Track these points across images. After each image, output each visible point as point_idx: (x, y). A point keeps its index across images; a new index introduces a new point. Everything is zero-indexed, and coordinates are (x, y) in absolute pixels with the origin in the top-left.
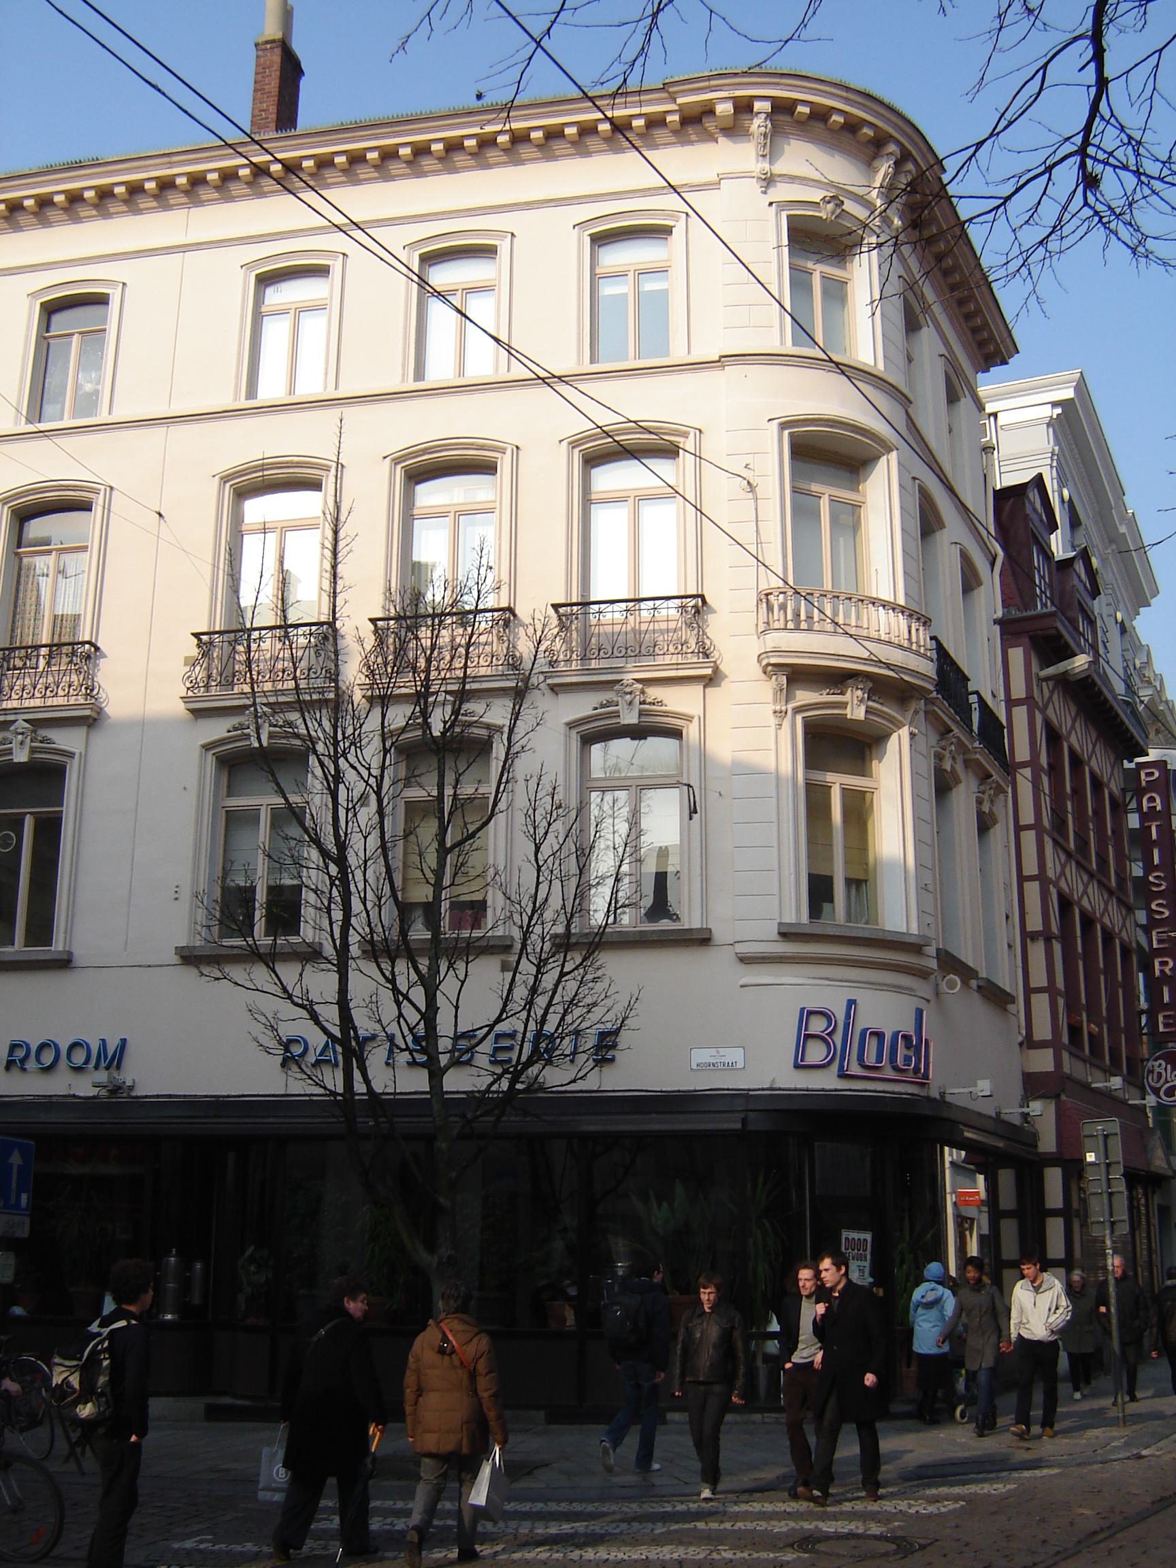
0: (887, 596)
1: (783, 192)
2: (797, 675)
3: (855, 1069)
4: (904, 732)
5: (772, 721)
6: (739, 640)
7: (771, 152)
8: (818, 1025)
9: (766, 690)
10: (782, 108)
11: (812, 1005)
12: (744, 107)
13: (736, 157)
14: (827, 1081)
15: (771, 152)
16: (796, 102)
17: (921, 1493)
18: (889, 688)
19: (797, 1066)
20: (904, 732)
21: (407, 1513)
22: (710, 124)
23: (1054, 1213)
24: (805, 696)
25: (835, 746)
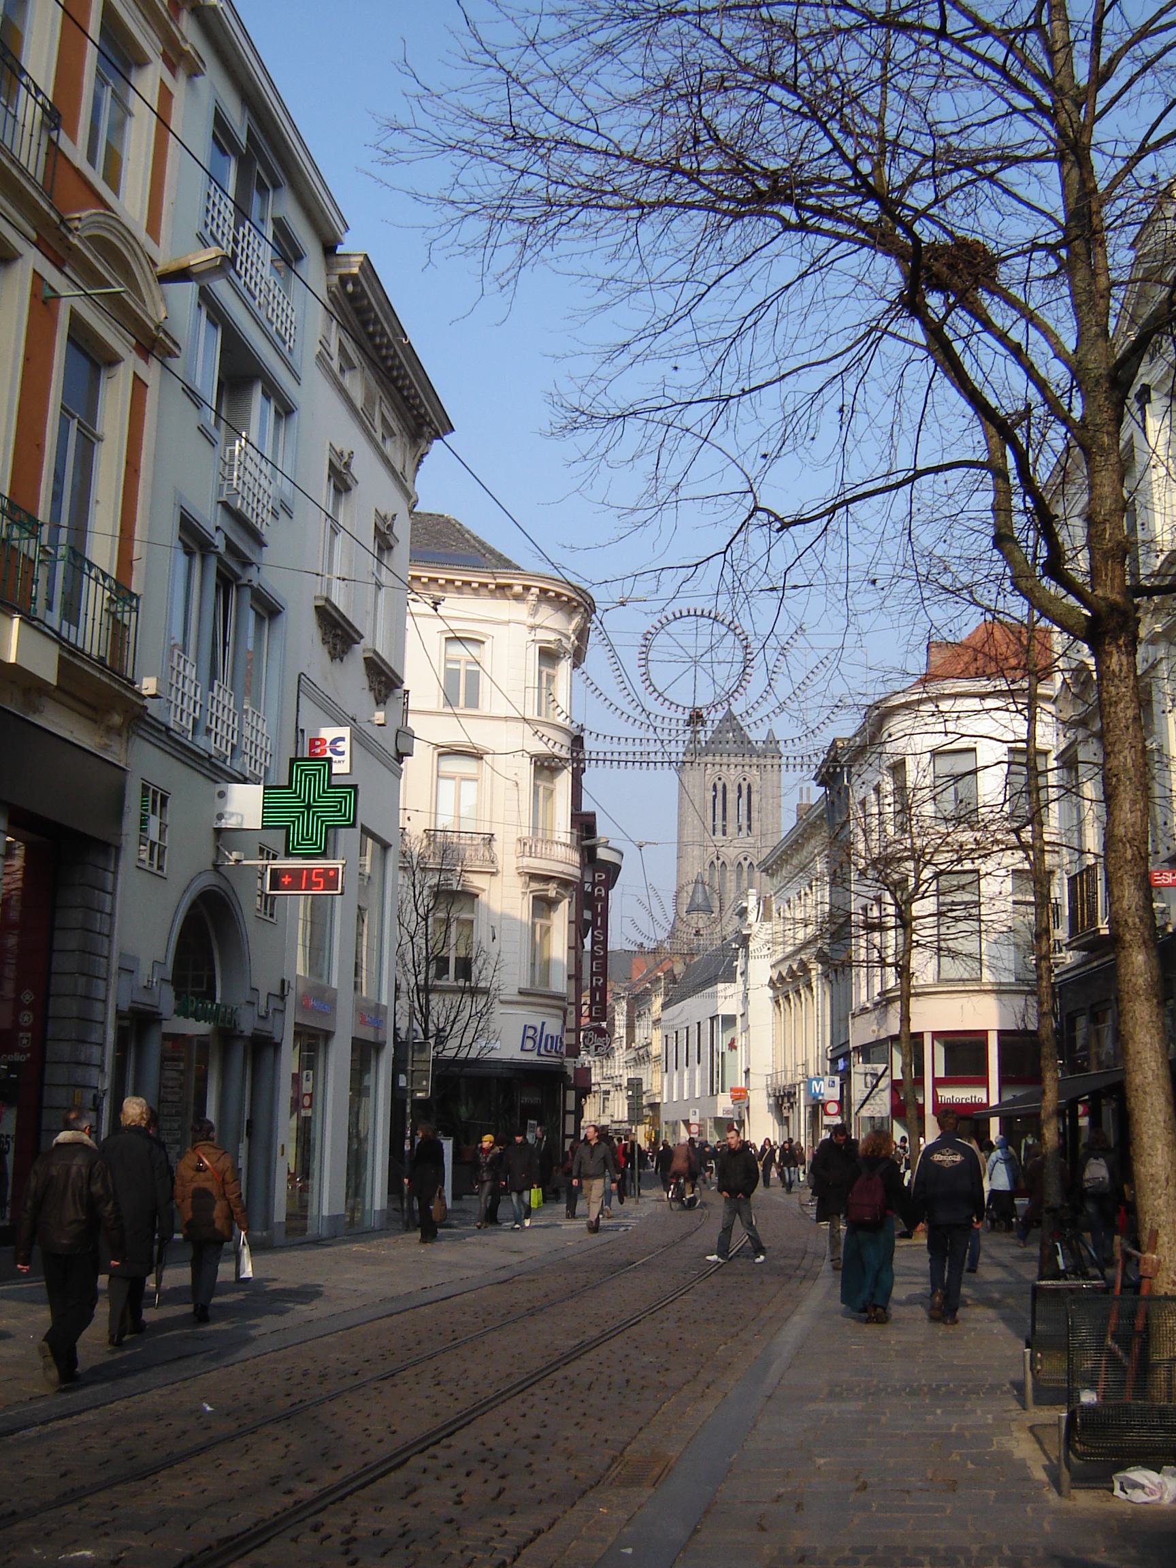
0: (562, 840)
1: (542, 635)
2: (534, 877)
3: (543, 1051)
4: (566, 901)
5: (520, 896)
6: (508, 857)
7: (534, 614)
8: (530, 1032)
9: (519, 882)
10: (544, 591)
11: (529, 1024)
12: (527, 588)
13: (519, 611)
14: (532, 1057)
15: (534, 614)
16: (549, 590)
17: (776, 209)
18: (564, 883)
19: (522, 1050)
20: (566, 901)
21: (1112, 592)
22: (508, 593)
23: (570, 1112)
24: (534, 886)
25: (544, 905)
